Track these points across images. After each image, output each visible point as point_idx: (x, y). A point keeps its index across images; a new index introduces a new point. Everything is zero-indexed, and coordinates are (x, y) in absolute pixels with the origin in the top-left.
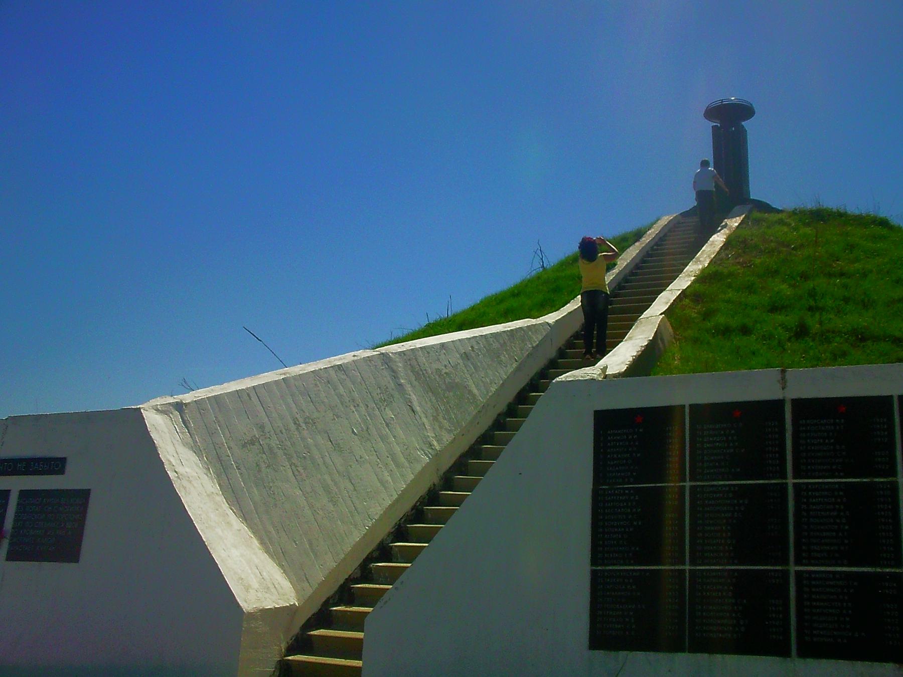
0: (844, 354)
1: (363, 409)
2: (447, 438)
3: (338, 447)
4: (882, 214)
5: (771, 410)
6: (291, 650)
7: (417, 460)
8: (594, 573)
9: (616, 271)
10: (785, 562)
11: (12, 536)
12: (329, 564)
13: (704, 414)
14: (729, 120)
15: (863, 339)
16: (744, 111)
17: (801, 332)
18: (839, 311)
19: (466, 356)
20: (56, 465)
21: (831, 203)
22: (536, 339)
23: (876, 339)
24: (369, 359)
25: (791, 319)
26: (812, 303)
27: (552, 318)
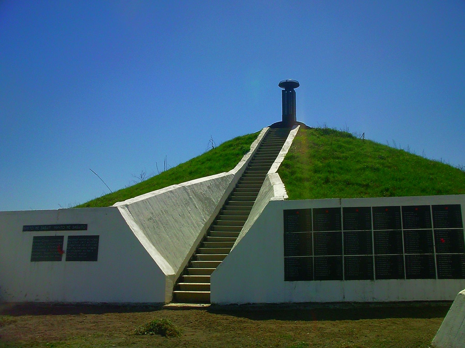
0: (343, 190)
1: (181, 207)
2: (208, 218)
3: (176, 221)
4: (350, 132)
5: (336, 211)
6: (174, 290)
7: (199, 226)
8: (285, 259)
9: (251, 153)
10: (342, 254)
11: (67, 252)
12: (181, 261)
13: (317, 211)
14: (289, 88)
15: (348, 184)
16: (296, 85)
17: (327, 181)
18: (339, 173)
19: (209, 187)
20: (84, 227)
21: (330, 126)
22: (230, 180)
23: (353, 184)
24: (179, 188)
25: (323, 175)
26: (329, 169)
27: (233, 172)
